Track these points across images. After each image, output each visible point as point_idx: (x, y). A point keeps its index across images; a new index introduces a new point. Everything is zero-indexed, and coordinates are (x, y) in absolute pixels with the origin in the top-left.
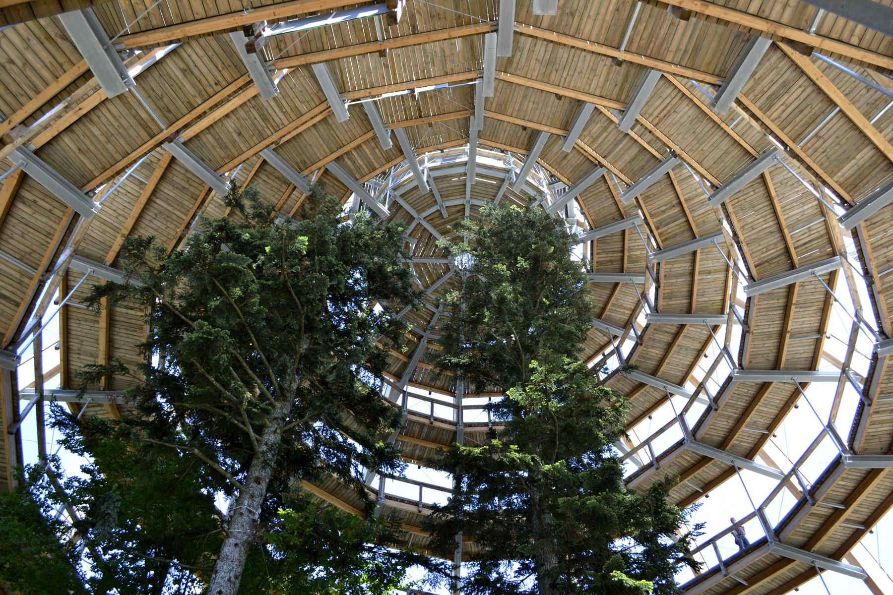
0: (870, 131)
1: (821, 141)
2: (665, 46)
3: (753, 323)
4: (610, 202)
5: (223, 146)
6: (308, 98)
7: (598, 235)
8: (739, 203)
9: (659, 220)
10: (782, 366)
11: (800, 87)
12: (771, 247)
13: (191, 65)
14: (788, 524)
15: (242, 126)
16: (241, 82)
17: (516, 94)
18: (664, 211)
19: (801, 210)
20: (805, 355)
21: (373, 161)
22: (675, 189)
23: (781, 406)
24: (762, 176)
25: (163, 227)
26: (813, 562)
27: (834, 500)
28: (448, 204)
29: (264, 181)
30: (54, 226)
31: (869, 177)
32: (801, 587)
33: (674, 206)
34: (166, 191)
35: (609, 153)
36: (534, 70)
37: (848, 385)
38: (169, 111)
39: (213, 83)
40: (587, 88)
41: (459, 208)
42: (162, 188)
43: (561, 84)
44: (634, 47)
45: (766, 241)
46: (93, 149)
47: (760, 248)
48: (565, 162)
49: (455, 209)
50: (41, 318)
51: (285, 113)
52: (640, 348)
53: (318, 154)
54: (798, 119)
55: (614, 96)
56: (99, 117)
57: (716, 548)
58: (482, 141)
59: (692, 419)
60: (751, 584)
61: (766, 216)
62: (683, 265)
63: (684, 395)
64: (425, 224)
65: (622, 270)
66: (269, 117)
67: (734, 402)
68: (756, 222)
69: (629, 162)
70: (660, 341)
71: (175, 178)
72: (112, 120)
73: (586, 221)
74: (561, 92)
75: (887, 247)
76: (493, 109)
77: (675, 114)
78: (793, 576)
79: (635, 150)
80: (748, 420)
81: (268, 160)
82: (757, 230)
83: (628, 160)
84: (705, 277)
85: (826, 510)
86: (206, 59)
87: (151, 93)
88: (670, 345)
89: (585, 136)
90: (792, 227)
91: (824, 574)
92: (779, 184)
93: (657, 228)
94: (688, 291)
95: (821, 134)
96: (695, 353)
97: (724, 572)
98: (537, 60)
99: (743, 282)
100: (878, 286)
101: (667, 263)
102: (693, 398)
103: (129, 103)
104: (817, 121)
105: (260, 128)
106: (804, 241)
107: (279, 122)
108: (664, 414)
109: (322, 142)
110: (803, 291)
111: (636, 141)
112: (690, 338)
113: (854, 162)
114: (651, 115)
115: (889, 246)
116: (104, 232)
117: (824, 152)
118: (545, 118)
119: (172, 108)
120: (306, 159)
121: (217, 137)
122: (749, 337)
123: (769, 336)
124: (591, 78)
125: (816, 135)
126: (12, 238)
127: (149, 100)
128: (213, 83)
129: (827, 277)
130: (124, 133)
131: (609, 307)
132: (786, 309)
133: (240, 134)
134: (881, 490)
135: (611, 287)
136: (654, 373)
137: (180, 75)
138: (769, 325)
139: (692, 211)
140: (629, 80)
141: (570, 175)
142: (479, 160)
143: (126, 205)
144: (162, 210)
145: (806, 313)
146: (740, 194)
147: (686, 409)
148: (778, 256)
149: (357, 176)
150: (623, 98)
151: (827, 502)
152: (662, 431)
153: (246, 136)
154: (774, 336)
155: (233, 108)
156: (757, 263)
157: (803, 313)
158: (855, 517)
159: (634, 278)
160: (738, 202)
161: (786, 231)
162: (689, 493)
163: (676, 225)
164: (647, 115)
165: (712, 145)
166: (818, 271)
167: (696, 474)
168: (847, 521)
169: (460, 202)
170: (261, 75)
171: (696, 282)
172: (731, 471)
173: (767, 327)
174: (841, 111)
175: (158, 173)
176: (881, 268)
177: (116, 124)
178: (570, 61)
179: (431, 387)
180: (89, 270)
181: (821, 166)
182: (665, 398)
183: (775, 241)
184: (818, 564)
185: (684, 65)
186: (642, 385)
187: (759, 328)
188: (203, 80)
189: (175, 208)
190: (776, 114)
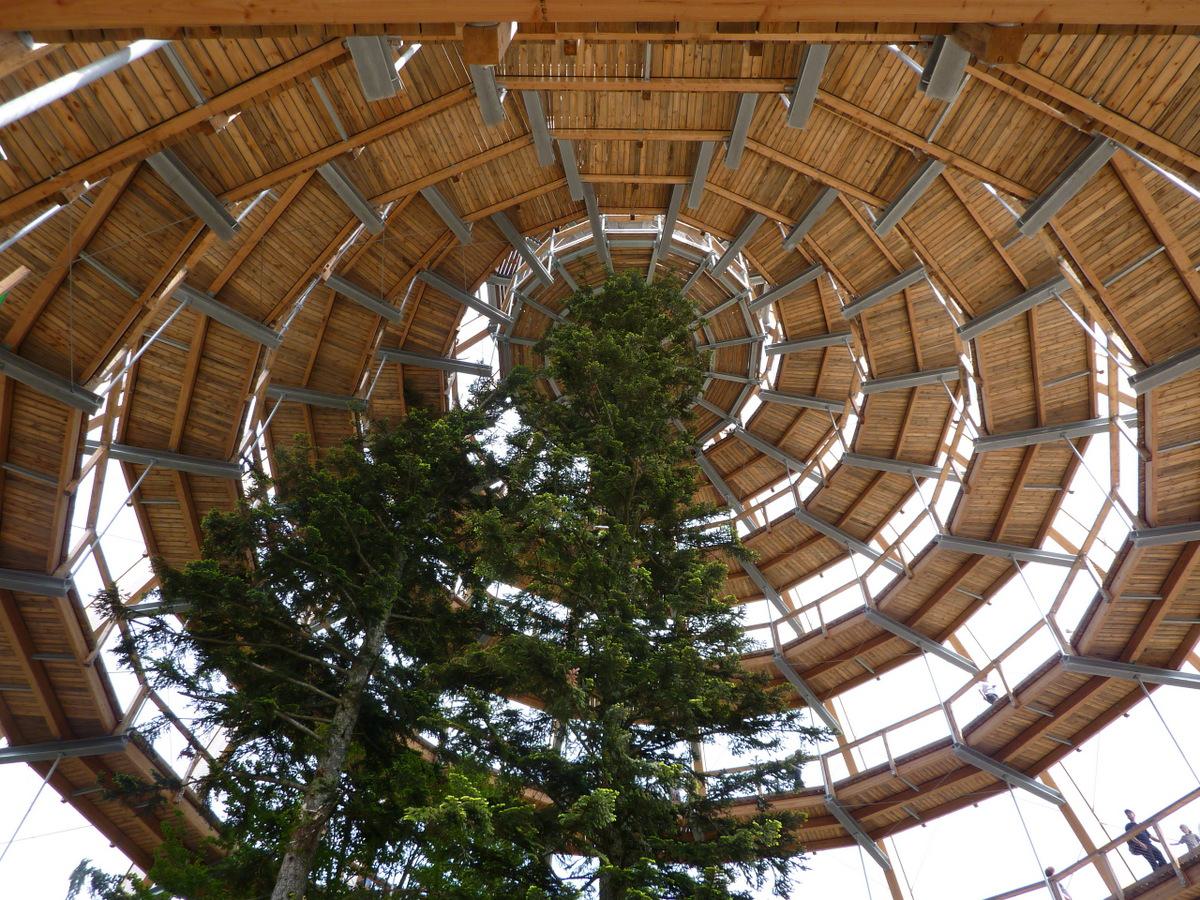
4: (815, 308)
17: (482, 177)
18: (761, 183)
29: (325, 420)
32: (982, 804)
34: (203, 499)
57: (819, 609)
59: (944, 510)
71: (202, 484)
73: (779, 326)
86: (40, 406)
99: (971, 432)
107: (239, 380)
117: (695, 57)
126: (44, 639)
131: (827, 314)
133: (217, 413)
137: (34, 432)
138: (962, 245)
146: (770, 126)
176: (1165, 441)
178: (439, 132)
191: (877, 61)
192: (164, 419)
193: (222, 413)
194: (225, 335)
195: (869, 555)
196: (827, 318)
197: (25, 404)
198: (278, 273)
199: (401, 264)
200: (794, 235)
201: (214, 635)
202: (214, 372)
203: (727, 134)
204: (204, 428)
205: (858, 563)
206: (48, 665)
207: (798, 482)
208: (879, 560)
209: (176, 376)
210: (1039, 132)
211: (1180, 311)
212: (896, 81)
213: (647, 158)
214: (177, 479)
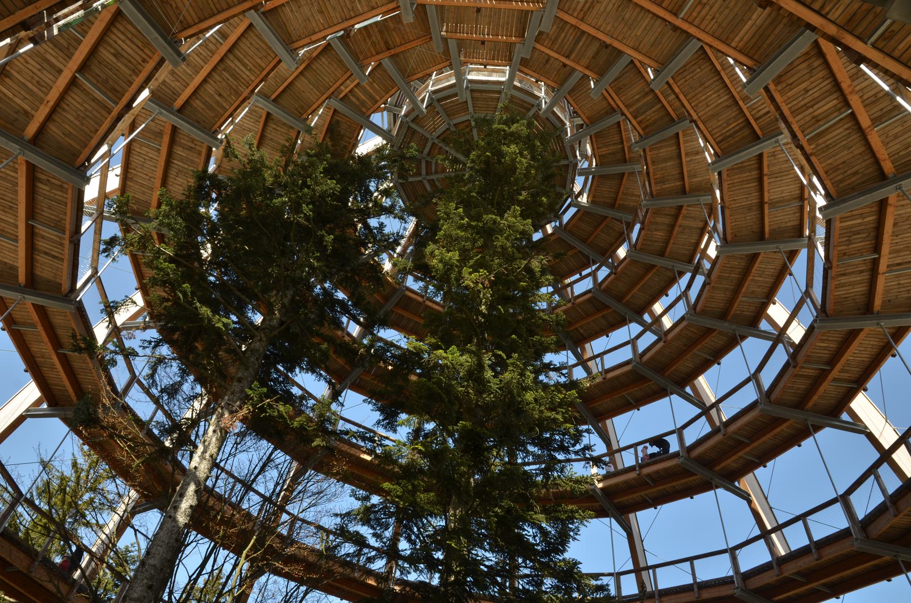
1: (708, 7)
5: (211, 108)
6: (265, 54)
8: (687, 83)
9: (636, 109)
13: (119, 49)
14: (776, 386)
15: (220, 88)
18: (638, 100)
20: (792, 224)
21: (374, 94)
26: (806, 420)
28: (455, 121)
29: (274, 129)
33: (647, 93)
35: (571, 52)
38: (117, 91)
41: (466, 124)
42: (175, 151)
45: (724, 116)
47: (719, 123)
48: (548, 66)
51: (250, 70)
53: (312, 98)
56: (68, 105)
59: (693, 294)
60: (752, 442)
61: (718, 91)
65: (625, 161)
66: (237, 75)
67: (727, 275)
68: (710, 98)
69: (593, 57)
71: (182, 141)
72: (78, 106)
75: (812, 106)
80: (743, 290)
82: (712, 106)
83: (591, 56)
84: (694, 158)
85: (813, 371)
86: (128, 42)
87: (98, 78)
88: (672, 226)
93: (635, 118)
94: (679, 173)
97: (723, 431)
101: (651, 150)
105: (235, 87)
109: (312, 87)
110: (776, 161)
112: (691, 217)
113: (750, 23)
114: (575, 10)
115: (814, 105)
116: (144, 193)
117: (713, 18)
120: (302, 104)
123: (750, 209)
126: (43, 211)
130: (91, 115)
131: (619, 197)
133: (220, 95)
134: (869, 349)
137: (114, 60)
138: (746, 198)
141: (556, 78)
145: (785, 181)
146: (685, 73)
148: (741, 129)
149: (364, 110)
153: (225, 95)
155: (206, 74)
157: (780, 182)
158: (845, 376)
160: (686, 81)
163: (654, 112)
165: (645, 28)
166: (782, 139)
168: (835, 380)
170: (165, 48)
171: (684, 164)
173: (745, 200)
175: (166, 139)
177: (82, 109)
183: (734, 114)
186: (653, 266)
187: (737, 201)
188: (133, 60)
189: (189, 166)
191: (808, 75)
192: (178, 84)
193: (223, 97)
194: (254, 43)
195: (642, 322)
196: (618, 199)
197: (115, 35)
199: (382, 44)
200: (642, 143)
201: (183, 257)
202: (232, 66)
203: (660, 66)
204: (205, 103)
205: (635, 328)
206: (37, 231)
207: (598, 269)
208: (647, 328)
209: (203, 57)
211: (859, 293)
212: (811, 92)
213: (579, 50)
214: (168, 131)
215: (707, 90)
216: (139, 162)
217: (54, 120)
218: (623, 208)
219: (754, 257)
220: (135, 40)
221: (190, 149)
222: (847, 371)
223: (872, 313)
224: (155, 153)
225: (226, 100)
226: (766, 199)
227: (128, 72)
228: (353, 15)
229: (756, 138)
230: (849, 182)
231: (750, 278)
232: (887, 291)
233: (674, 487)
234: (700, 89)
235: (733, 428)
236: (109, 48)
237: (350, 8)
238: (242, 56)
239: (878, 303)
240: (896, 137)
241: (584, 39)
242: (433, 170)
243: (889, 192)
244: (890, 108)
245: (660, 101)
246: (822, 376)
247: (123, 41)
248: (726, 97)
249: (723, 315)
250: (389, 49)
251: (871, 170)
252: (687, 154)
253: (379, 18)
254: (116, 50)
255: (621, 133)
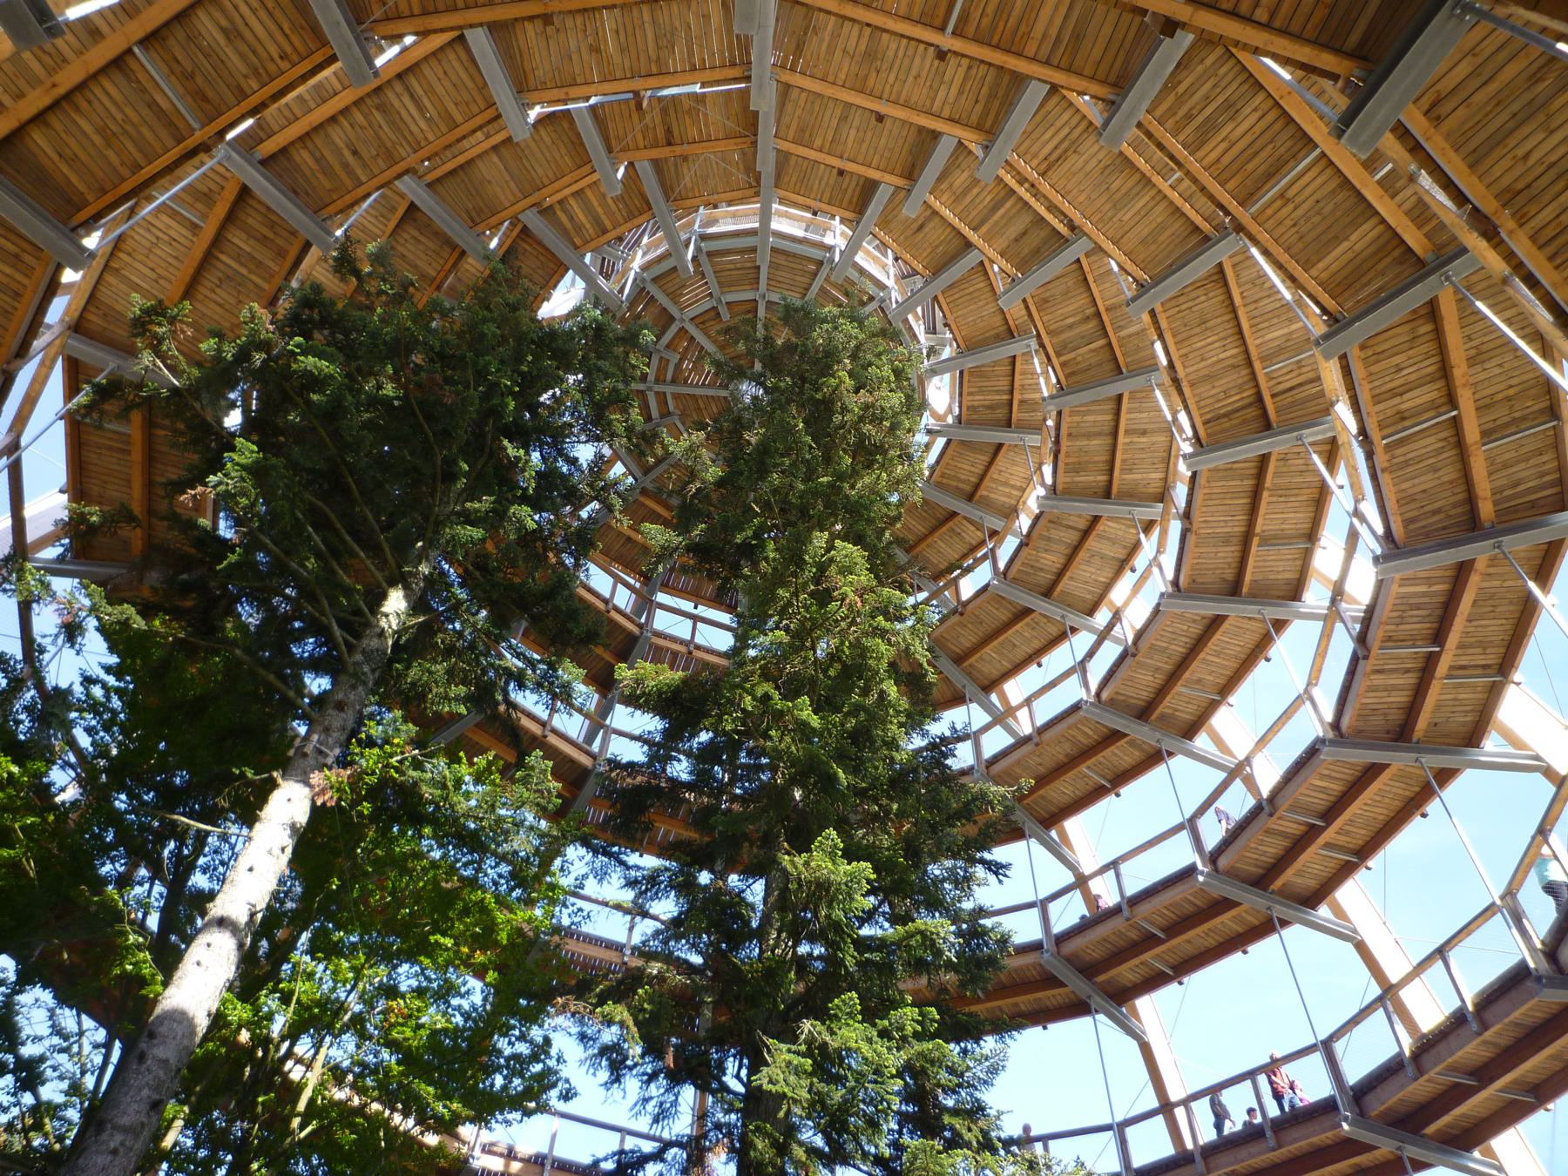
0: (1372, 194)
1: (1291, 206)
2: (1023, 29)
3: (1196, 516)
5: (328, 171)
7: (970, 363)
10: (1245, 590)
11: (1255, 110)
12: (1229, 392)
16: (318, 58)
17: (828, 113)
18: (1071, 327)
19: (1286, 331)
20: (1287, 576)
22: (1089, 289)
23: (1243, 656)
24: (1220, 268)
25: (233, 301)
27: (1306, 811)
30: (25, 281)
31: (1372, 273)
34: (236, 240)
35: (982, 222)
36: (840, 69)
37: (1339, 626)
39: (276, 56)
40: (928, 104)
43: (885, 96)
44: (971, 30)
46: (82, 155)
48: (920, 235)
49: (743, 308)
50: (19, 436)
51: (429, 121)
52: (1025, 551)
54: (1250, 167)
55: (974, 119)
56: (89, 102)
57: (1118, 875)
58: (782, 193)
62: (1099, 418)
63: (1091, 630)
64: (692, 330)
69: (1016, 240)
70: (1059, 542)
71: (250, 221)
72: (113, 109)
74: (884, 108)
75: (1401, 394)
76: (791, 137)
77: (1075, 157)
78: (1241, 930)
79: (1025, 220)
81: (417, 203)
83: (1014, 236)
87: (175, 65)
88: (1076, 549)
89: (943, 192)
90: (1267, 359)
91: (1287, 933)
92: (1249, 286)
93: (1058, 355)
95: (1290, 194)
96: (1117, 564)
98: (845, 51)
100: (1381, 459)
101: (1072, 413)
102: (1104, 635)
103: (138, 81)
104: (1283, 171)
105: (389, 145)
106: (1288, 385)
107: (419, 136)
108: (1059, 659)
111: (1026, 203)
113: (1345, 245)
118: (877, 158)
119: (210, 94)
121: (318, 154)
122: (1191, 539)
123: (1226, 540)
124: (935, 86)
125: (1282, 195)
127: (173, 78)
128: (276, 56)
129: (1328, 447)
130: (134, 133)
132: (1255, 496)
133: (355, 153)
135: (991, 450)
136: (1047, 593)
137: (222, 41)
139: (1117, 329)
140: (1000, 94)
142: (777, 225)
143: (170, 260)
144: (229, 272)
146: (1182, 300)
147: (1091, 654)
148: (1243, 408)
149: (578, 241)
150: (988, 124)
151: (1295, 812)
152: (1052, 684)
153: (365, 155)
154: (1235, 540)
155: (342, 105)
156: (1209, 416)
158: (1342, 840)
159: (1027, 437)
161: (1257, 365)
162: (1089, 788)
164: (1028, 157)
165: (1138, 212)
167: (1099, 757)
168: (1328, 846)
169: (749, 296)
171: (1120, 447)
172: (1154, 758)
174: (1323, 155)
175: (221, 210)
178: (900, 54)
179: (696, 596)
180: (112, 365)
181: (1287, 250)
182: (1061, 637)
184: (1278, 911)
185: (1031, 55)
186: (1027, 612)
188: (260, 50)
189: (250, 271)
190: (1214, 156)
193: (361, 158)
198: (585, 56)
199: (660, 132)
202: (397, 104)
210: (1448, 493)
214: (230, 194)
215: (1209, 333)
216: (144, 242)
217: (47, 125)
218: (988, 505)
219: (1216, 622)
220: (278, 14)
221: (263, 240)
222: (1347, 833)
223: (1409, 741)
224: (184, 231)
225: (365, 165)
226: (1258, 529)
227: (244, 69)
228: (655, 71)
229: (1266, 426)
230: (1424, 523)
231: (1202, 655)
232: (1438, 707)
233: (1016, 1005)
234: (1198, 330)
235: (1144, 909)
236: (218, 15)
237: (654, 57)
238: (420, 92)
239: (1422, 724)
240: (1505, 466)
241: (1008, 205)
242: (669, 376)
243: (1479, 552)
244: (1506, 419)
245: (1106, 335)
246: (1311, 833)
247: (254, 11)
248: (1235, 351)
249: (1143, 713)
250: (670, 144)
251: (1459, 510)
252: (1127, 432)
253: (697, 88)
254: (232, 22)
255: (1013, 375)
